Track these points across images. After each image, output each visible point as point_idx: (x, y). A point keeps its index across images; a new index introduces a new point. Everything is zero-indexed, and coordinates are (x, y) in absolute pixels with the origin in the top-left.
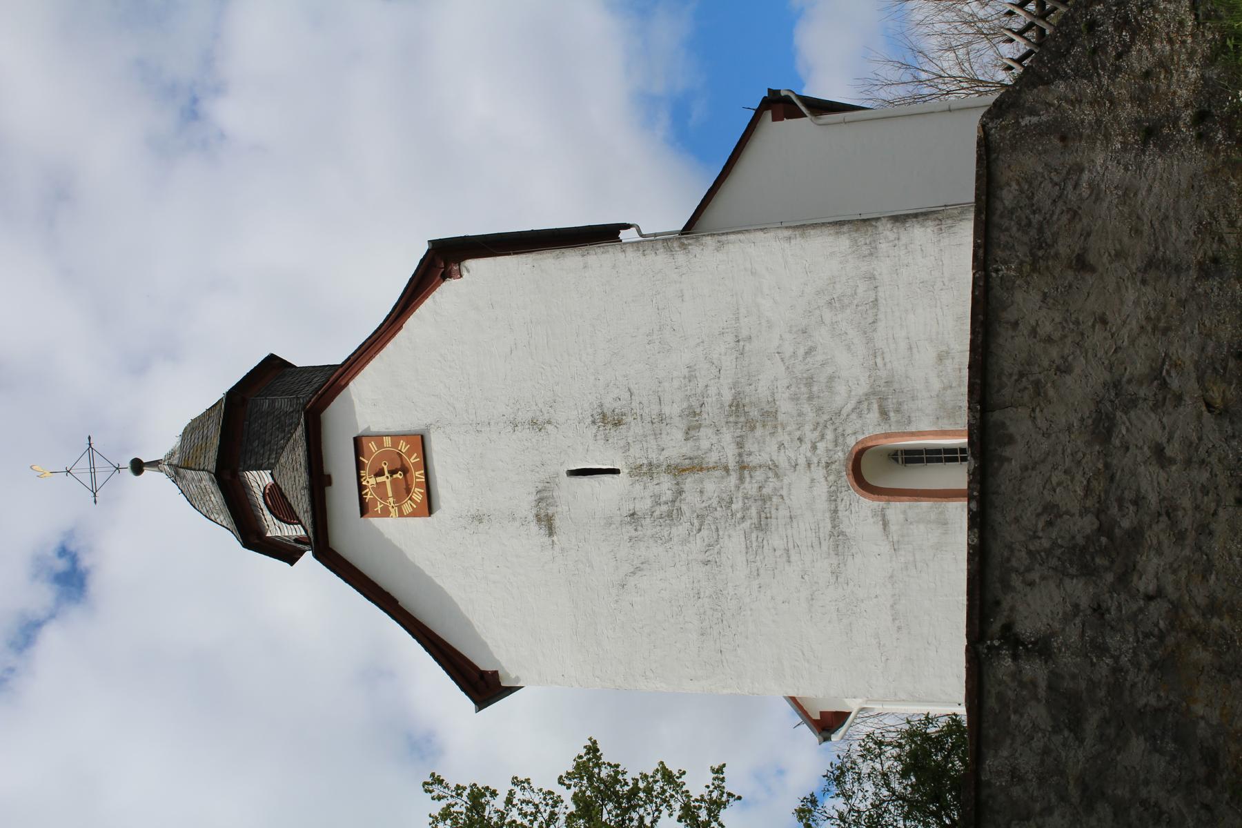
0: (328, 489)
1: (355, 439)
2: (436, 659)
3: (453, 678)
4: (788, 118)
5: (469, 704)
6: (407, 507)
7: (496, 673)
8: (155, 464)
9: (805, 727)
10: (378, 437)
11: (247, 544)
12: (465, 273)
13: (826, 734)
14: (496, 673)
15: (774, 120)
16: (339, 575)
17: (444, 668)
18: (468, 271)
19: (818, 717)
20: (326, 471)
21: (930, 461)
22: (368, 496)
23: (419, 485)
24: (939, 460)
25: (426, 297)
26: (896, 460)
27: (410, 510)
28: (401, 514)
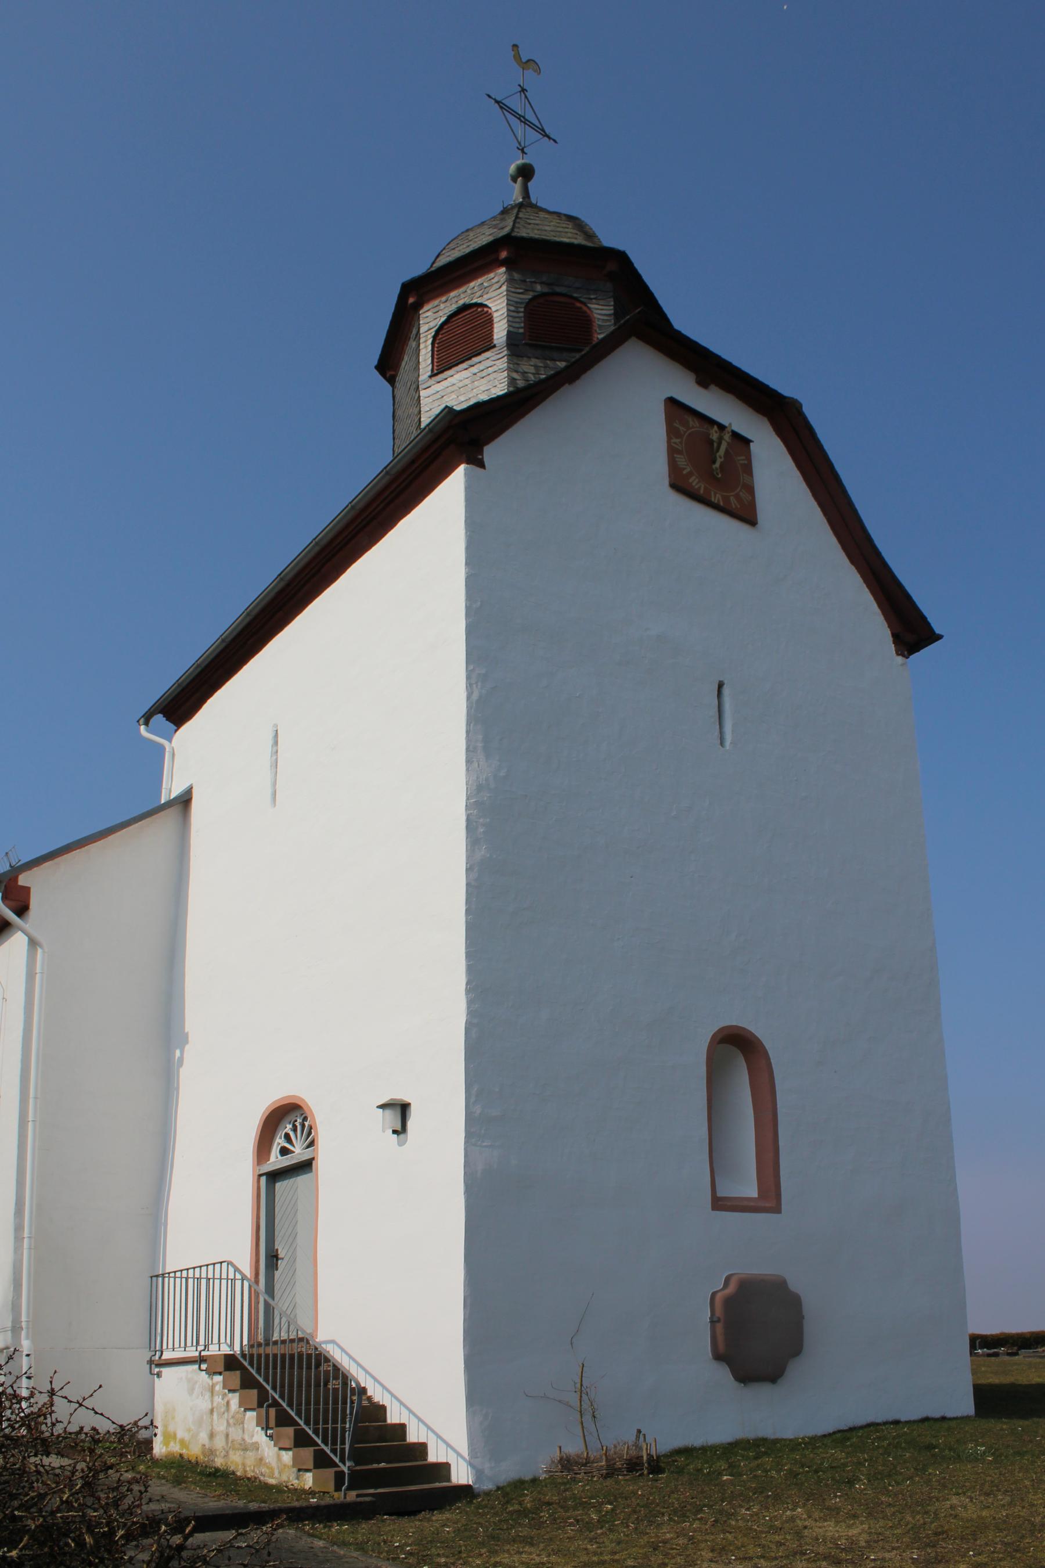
18: (902, 665)
20: (713, 387)
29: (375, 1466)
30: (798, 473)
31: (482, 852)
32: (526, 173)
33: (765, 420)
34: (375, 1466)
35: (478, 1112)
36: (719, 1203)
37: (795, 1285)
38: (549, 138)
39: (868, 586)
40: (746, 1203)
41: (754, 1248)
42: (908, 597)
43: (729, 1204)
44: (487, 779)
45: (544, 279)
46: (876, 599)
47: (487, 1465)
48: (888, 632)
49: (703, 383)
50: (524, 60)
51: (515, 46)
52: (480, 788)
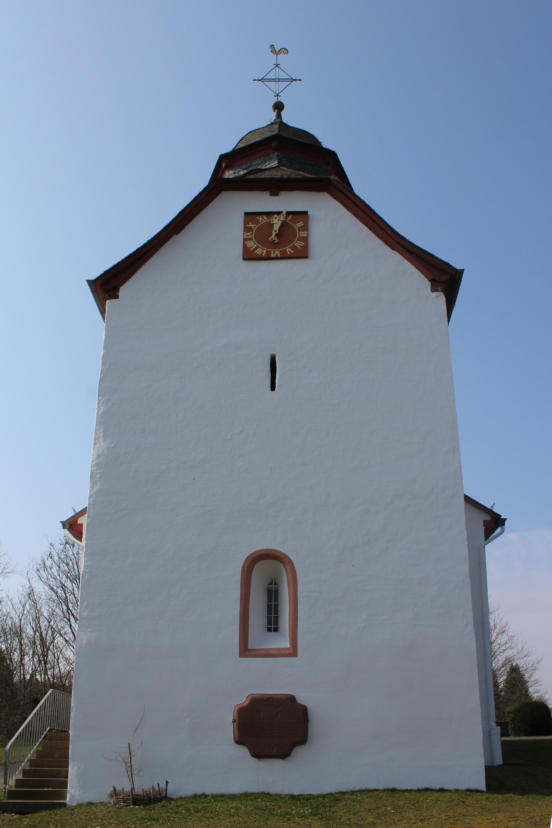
0: (268, 193)
1: (306, 213)
2: (130, 255)
3: (115, 266)
4: (485, 529)
5: (93, 276)
6: (251, 244)
7: (117, 297)
8: (279, 116)
9: (73, 514)
10: (305, 228)
11: (222, 158)
12: (435, 294)
13: (67, 525)
14: (117, 297)
15: (485, 522)
16: (201, 194)
17: (123, 261)
18: (437, 297)
19: (79, 521)
20: (281, 193)
21: (269, 607)
22: (261, 219)
23: (268, 253)
24: (269, 612)
25: (417, 268)
26: (271, 584)
27: (249, 246)
28: (245, 240)
29: (46, 789)
30: (350, 213)
31: (98, 486)
32: (279, 107)
33: (326, 193)
34: (46, 789)
35: (86, 615)
36: (293, 652)
37: (243, 700)
38: (295, 80)
39: (407, 259)
40: (272, 652)
41: (271, 678)
42: (433, 256)
43: (254, 653)
44: (103, 451)
45: (244, 167)
46: (413, 264)
47: (77, 793)
48: (427, 280)
49: (274, 193)
50: (277, 51)
51: (272, 46)
52: (98, 456)
